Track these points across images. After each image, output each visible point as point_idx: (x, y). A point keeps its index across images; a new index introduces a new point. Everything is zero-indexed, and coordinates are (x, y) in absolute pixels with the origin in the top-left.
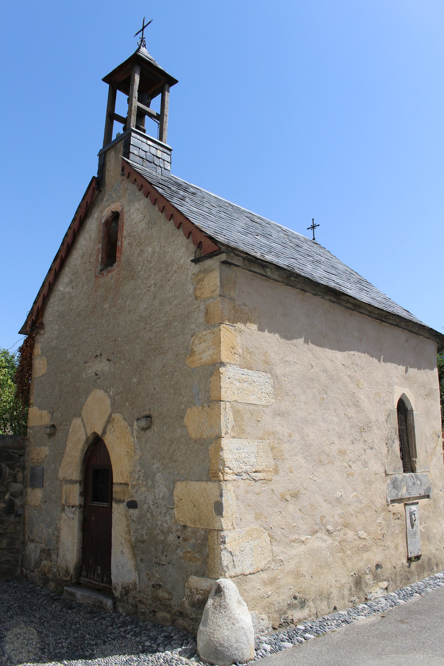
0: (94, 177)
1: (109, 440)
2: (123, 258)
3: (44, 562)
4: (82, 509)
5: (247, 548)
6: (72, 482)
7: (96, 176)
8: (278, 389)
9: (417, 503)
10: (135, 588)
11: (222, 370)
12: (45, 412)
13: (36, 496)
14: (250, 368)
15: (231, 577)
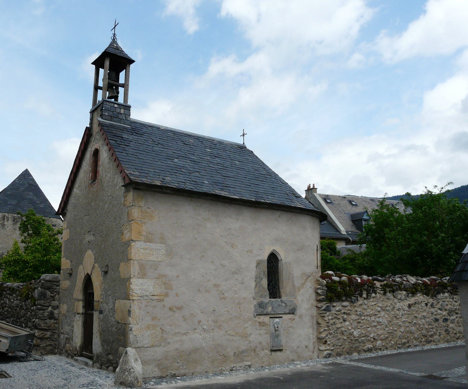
0: (87, 127)
1: (93, 278)
2: (99, 177)
3: (67, 345)
4: (84, 315)
5: (146, 335)
6: (78, 300)
7: (88, 126)
8: (170, 253)
9: (282, 317)
10: (101, 356)
11: (133, 244)
12: (68, 261)
13: (64, 308)
14: (150, 242)
15: (135, 348)
